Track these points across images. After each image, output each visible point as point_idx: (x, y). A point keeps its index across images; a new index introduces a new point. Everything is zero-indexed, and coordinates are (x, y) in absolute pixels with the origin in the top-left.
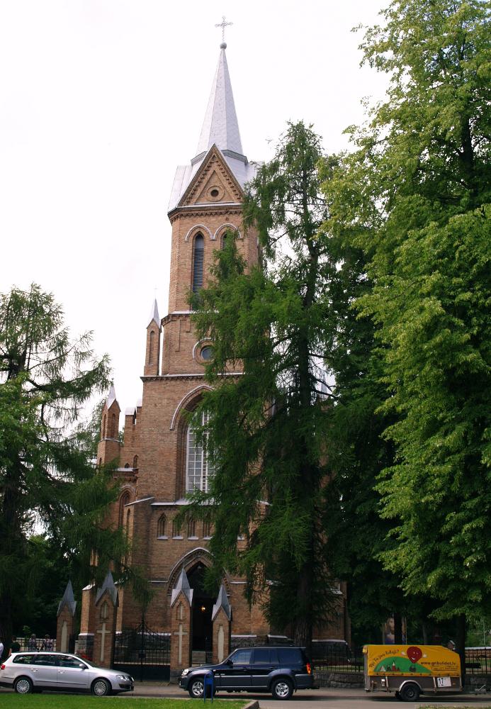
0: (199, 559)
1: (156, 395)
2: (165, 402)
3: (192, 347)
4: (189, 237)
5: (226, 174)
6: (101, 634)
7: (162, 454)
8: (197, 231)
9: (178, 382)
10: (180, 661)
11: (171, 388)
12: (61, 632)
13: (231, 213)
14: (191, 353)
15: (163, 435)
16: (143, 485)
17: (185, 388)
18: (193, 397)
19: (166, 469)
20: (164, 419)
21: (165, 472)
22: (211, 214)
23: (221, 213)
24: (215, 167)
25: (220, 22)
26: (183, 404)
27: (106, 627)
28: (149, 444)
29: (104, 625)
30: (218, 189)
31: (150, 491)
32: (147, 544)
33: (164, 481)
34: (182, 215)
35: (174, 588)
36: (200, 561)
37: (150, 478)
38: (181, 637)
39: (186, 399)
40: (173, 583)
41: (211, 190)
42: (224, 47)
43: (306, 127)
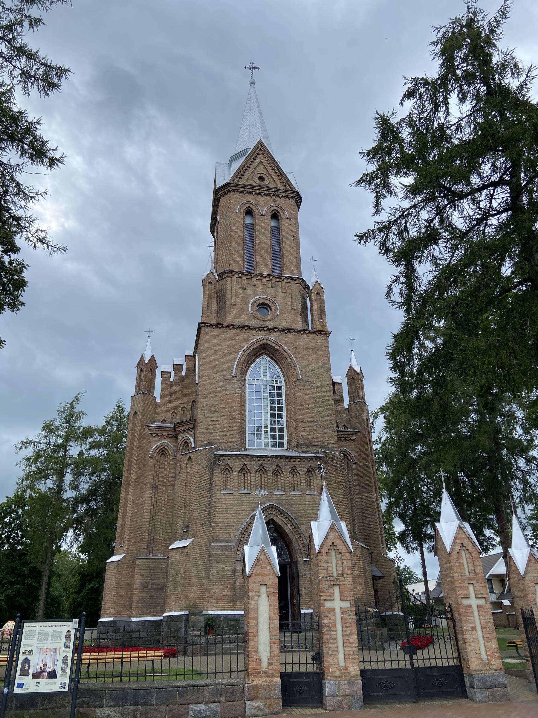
0: (272, 517)
1: (216, 341)
2: (225, 349)
3: (249, 303)
4: (240, 209)
5: (272, 164)
6: (333, 609)
7: (223, 400)
8: (248, 205)
9: (238, 331)
10: (484, 656)
11: (231, 336)
12: (256, 610)
13: (278, 196)
14: (248, 308)
15: (224, 380)
16: (203, 432)
17: (246, 337)
18: (255, 346)
19: (229, 416)
20: (225, 366)
21: (228, 420)
22: (260, 194)
23: (269, 195)
24: (261, 157)
25: (249, 65)
26: (244, 352)
27: (341, 593)
28: (209, 389)
29: (337, 590)
30: (264, 176)
31: (212, 438)
32: (211, 497)
33: (228, 430)
34: (233, 190)
35: (247, 544)
36: (272, 519)
37: (212, 424)
38: (475, 608)
39: (248, 348)
40: (243, 540)
41: (259, 175)
42: (252, 83)
43: (439, 48)
